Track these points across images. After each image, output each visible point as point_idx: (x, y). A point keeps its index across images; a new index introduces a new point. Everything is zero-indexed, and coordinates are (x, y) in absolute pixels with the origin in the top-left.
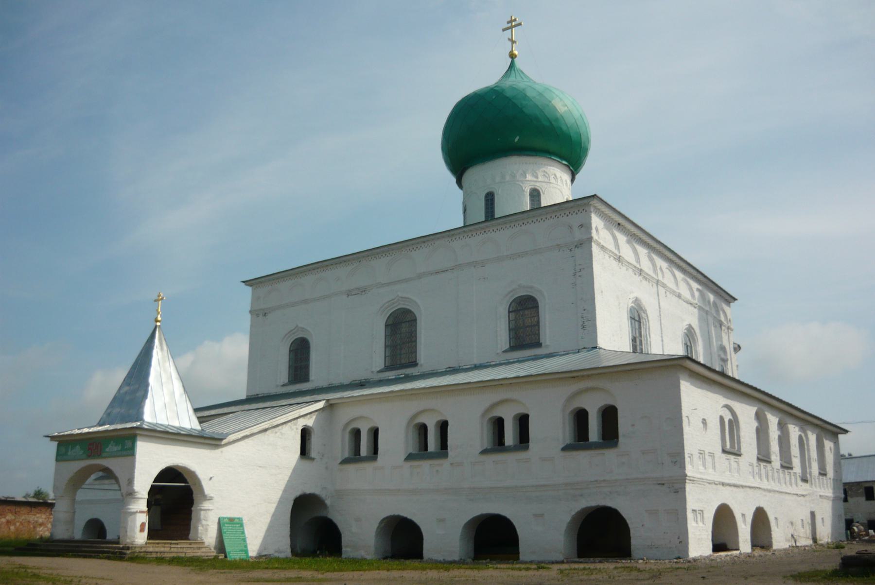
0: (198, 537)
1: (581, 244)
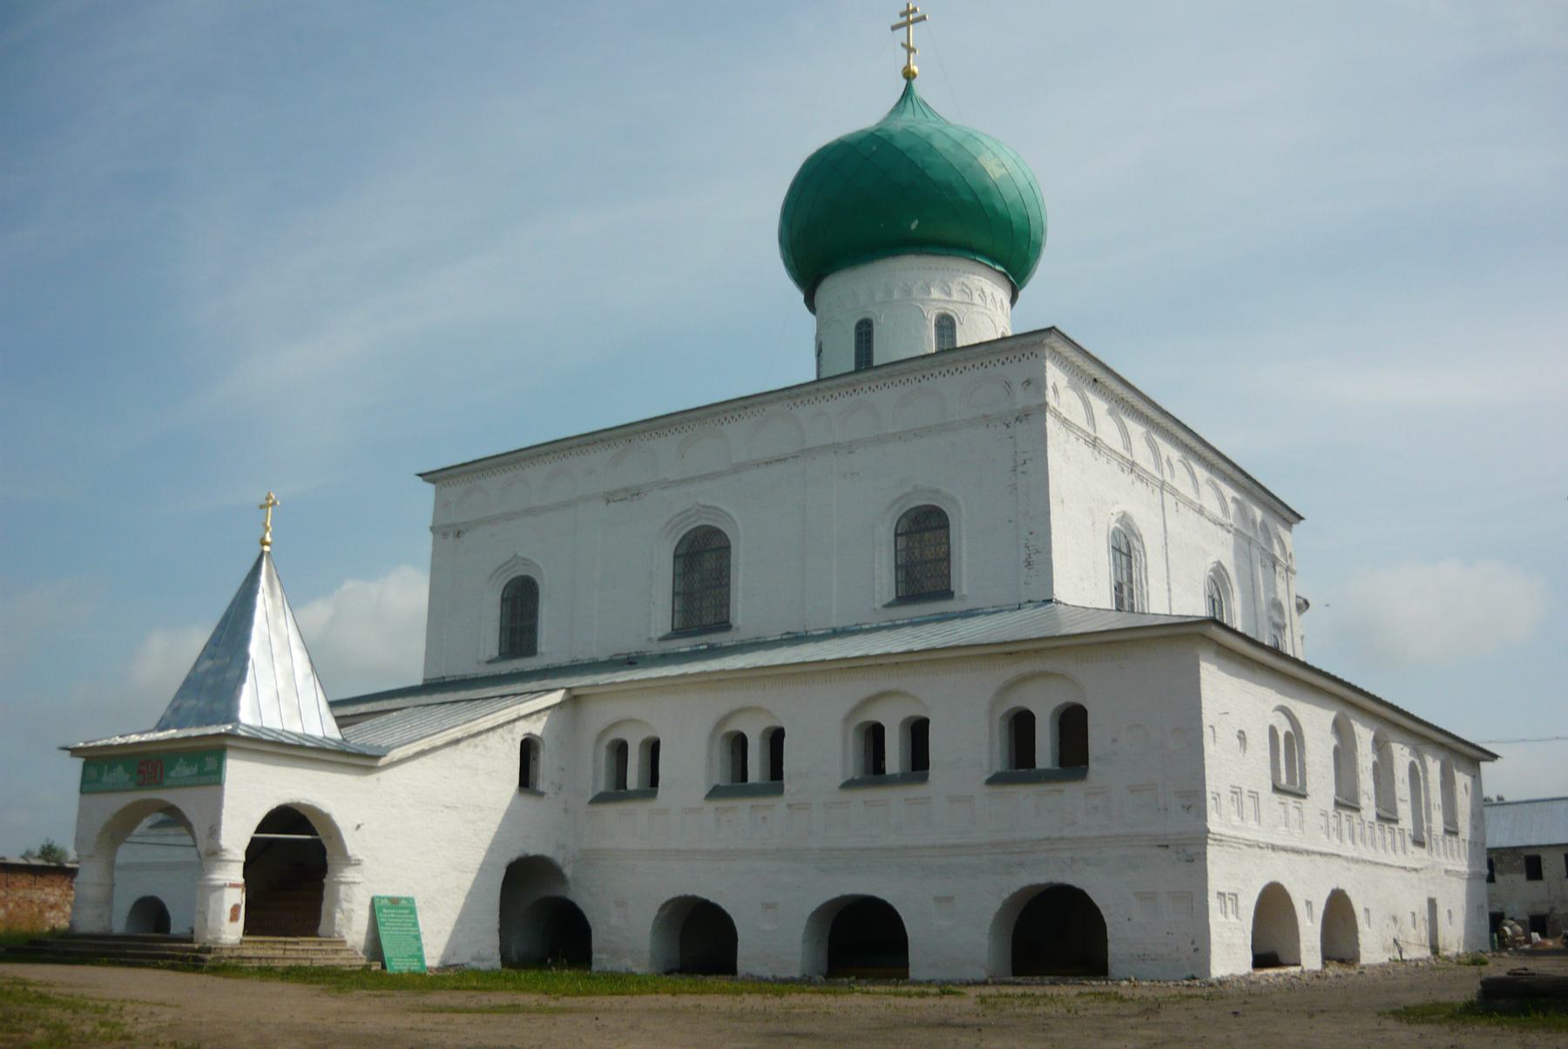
0: (334, 932)
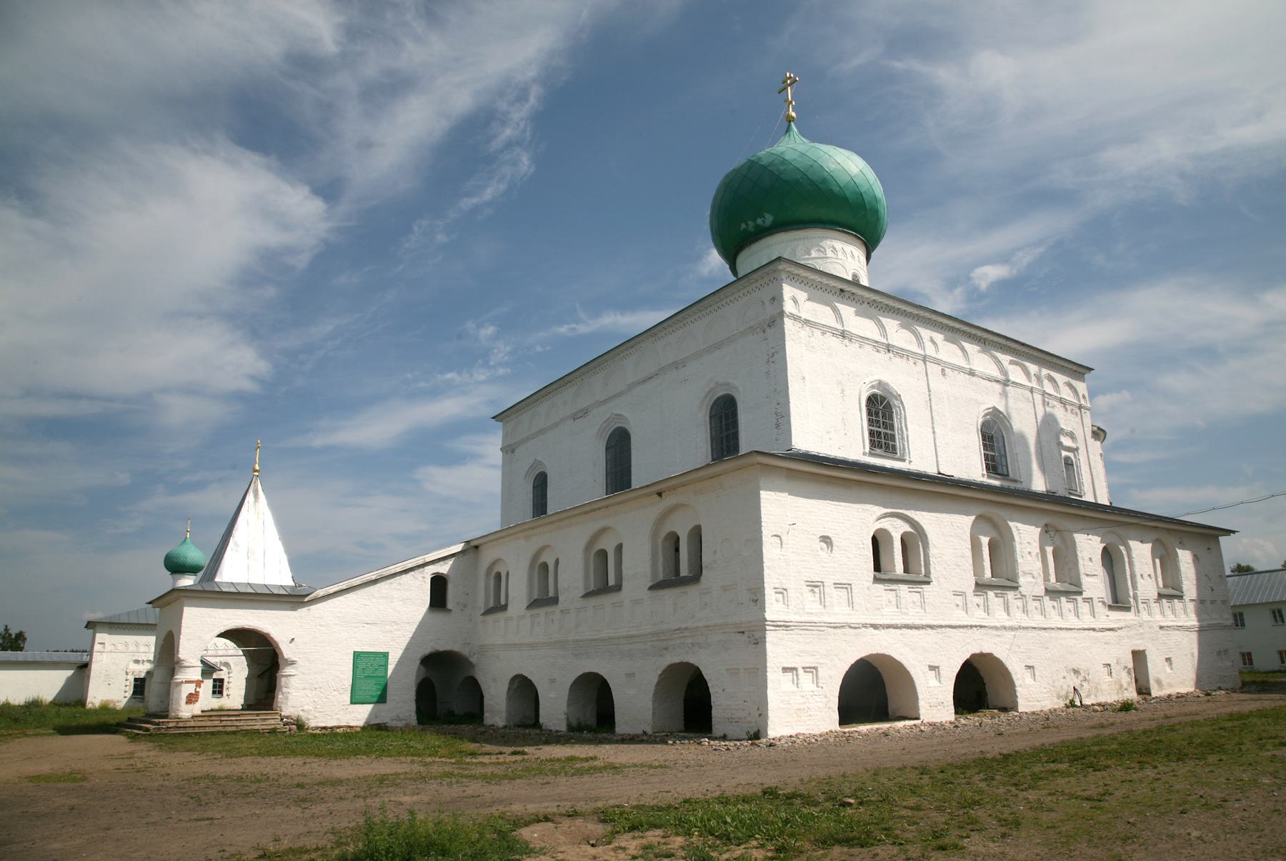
1: (773, 322)
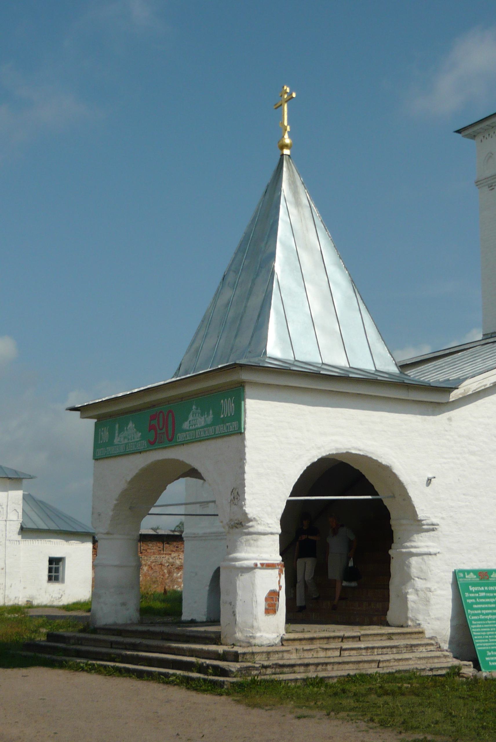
0: (407, 618)
